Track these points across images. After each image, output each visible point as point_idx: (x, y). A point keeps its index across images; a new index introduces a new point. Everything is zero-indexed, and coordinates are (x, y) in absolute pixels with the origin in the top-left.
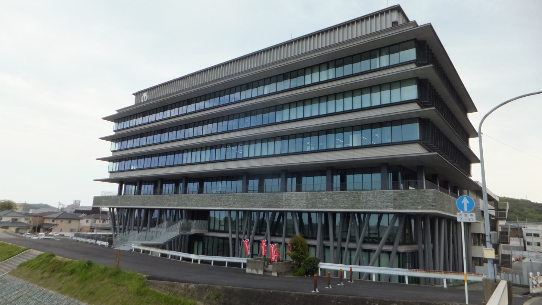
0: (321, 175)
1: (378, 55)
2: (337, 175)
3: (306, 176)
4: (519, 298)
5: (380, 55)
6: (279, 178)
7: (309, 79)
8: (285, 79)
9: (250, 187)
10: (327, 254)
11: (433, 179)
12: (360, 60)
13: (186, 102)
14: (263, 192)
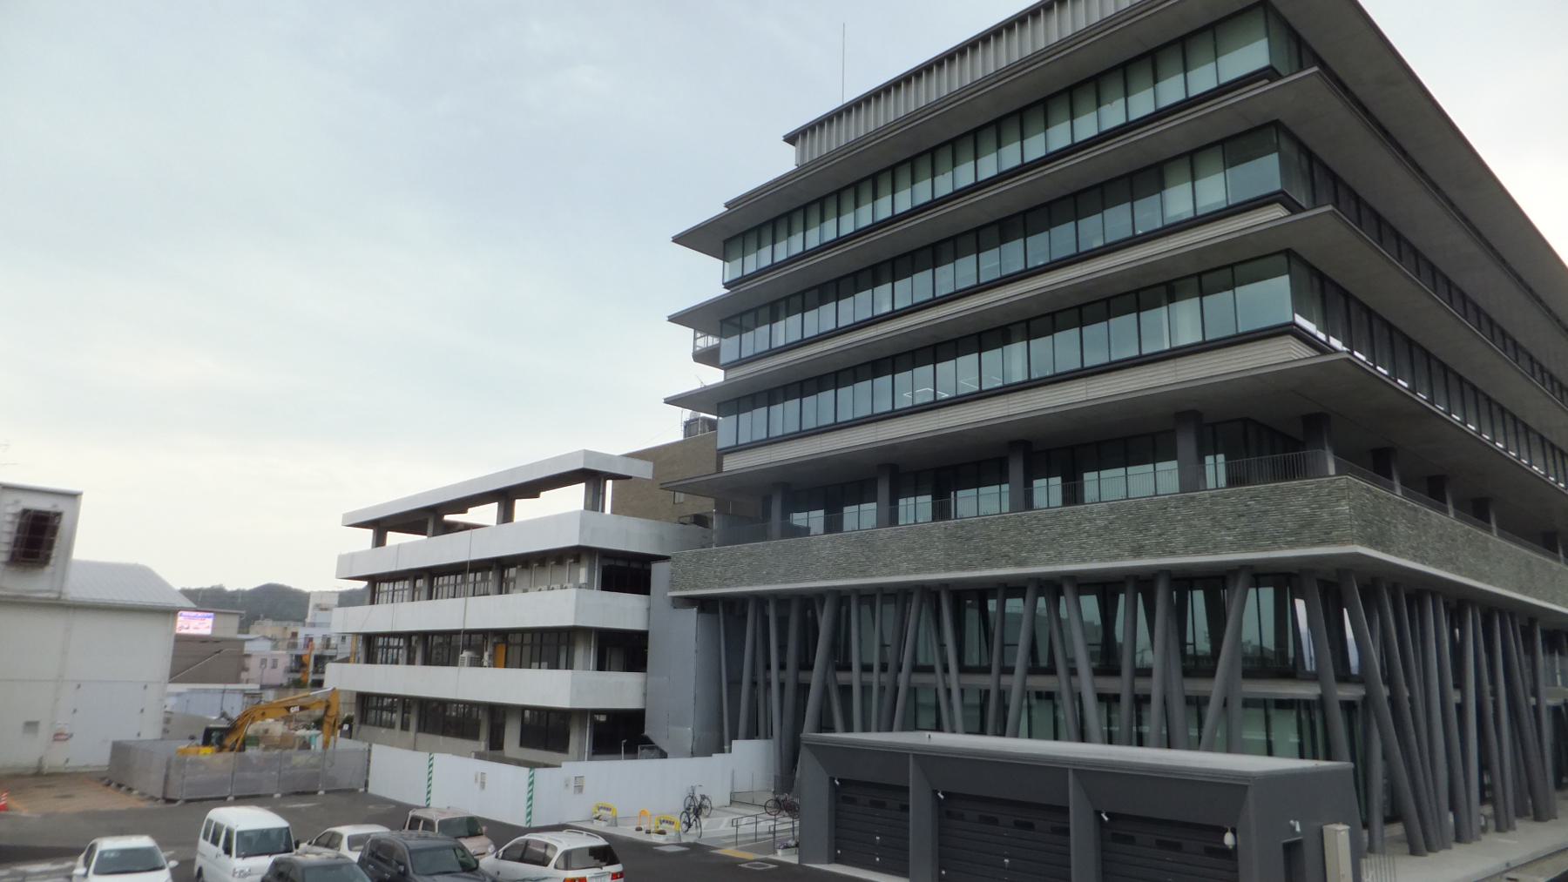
0: (1154, 460)
1: (782, 313)
2: (1215, 453)
3: (1099, 469)
4: (242, 799)
5: (956, 257)
6: (1000, 483)
7: (1178, 201)
8: (1004, 239)
9: (1039, 498)
10: (1114, 716)
11: (1378, 462)
12: (1102, 207)
13: (765, 312)
14: (1083, 502)
